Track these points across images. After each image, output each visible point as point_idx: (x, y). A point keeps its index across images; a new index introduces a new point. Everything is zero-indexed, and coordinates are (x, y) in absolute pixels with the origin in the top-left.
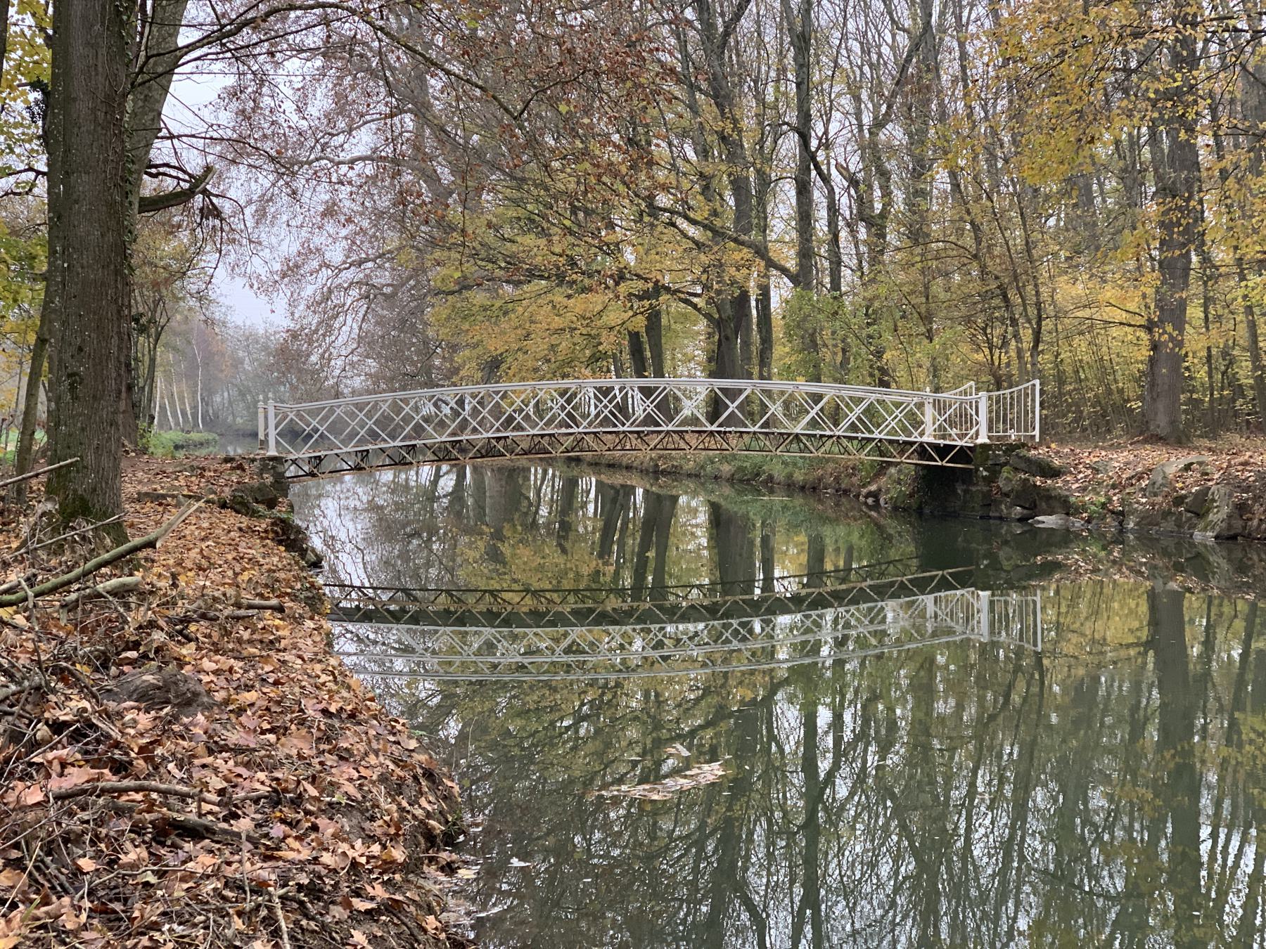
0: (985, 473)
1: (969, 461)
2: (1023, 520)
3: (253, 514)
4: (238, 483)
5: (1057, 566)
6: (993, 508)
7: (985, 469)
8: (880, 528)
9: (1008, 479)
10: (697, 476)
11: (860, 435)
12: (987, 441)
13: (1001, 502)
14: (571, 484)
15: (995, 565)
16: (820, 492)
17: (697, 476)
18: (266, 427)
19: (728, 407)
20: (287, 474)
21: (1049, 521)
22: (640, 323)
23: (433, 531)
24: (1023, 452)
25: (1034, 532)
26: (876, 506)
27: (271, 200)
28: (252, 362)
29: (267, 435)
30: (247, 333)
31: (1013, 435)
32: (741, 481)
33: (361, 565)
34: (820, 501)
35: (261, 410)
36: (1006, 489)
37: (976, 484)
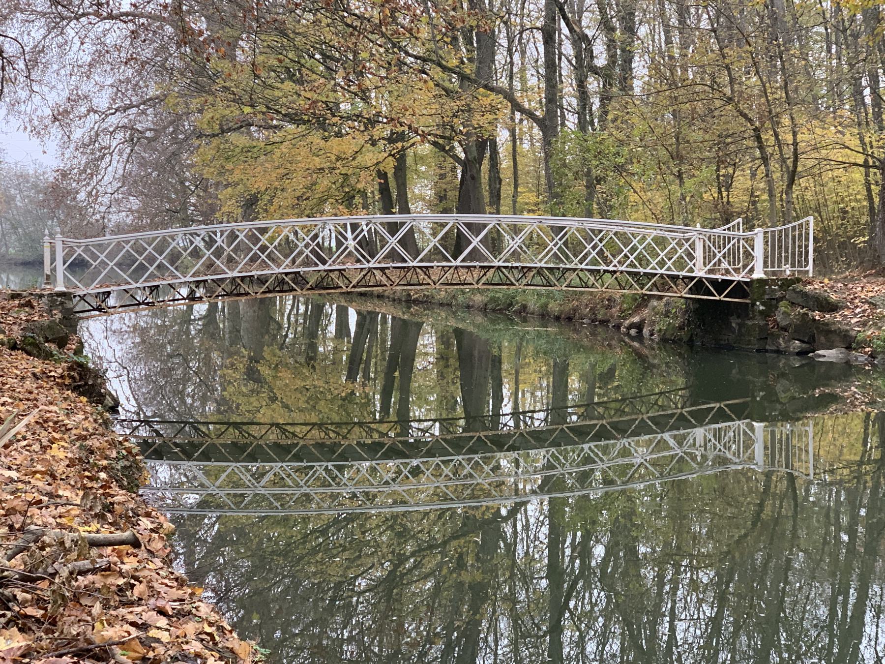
0: (761, 308)
1: (745, 295)
2: (802, 354)
3: (47, 356)
4: (27, 321)
5: (834, 398)
6: (769, 341)
7: (762, 304)
8: (640, 356)
9: (785, 314)
10: (449, 305)
11: (561, 265)
12: (763, 276)
13: (778, 336)
14: (318, 310)
15: (772, 397)
16: (580, 322)
17: (449, 305)
18: (53, 260)
19: (245, 236)
20: (77, 309)
21: (830, 355)
22: (389, 166)
23: (190, 348)
24: (799, 287)
25: (813, 365)
26: (639, 337)
27: (42, 51)
28: (23, 198)
29: (54, 270)
30: (18, 173)
31: (787, 270)
32: (494, 310)
33: (126, 383)
34: (575, 331)
35: (47, 245)
36: (784, 323)
37: (753, 318)
